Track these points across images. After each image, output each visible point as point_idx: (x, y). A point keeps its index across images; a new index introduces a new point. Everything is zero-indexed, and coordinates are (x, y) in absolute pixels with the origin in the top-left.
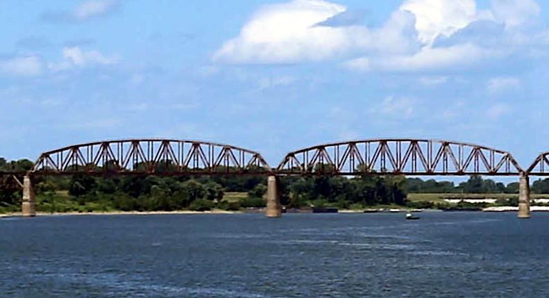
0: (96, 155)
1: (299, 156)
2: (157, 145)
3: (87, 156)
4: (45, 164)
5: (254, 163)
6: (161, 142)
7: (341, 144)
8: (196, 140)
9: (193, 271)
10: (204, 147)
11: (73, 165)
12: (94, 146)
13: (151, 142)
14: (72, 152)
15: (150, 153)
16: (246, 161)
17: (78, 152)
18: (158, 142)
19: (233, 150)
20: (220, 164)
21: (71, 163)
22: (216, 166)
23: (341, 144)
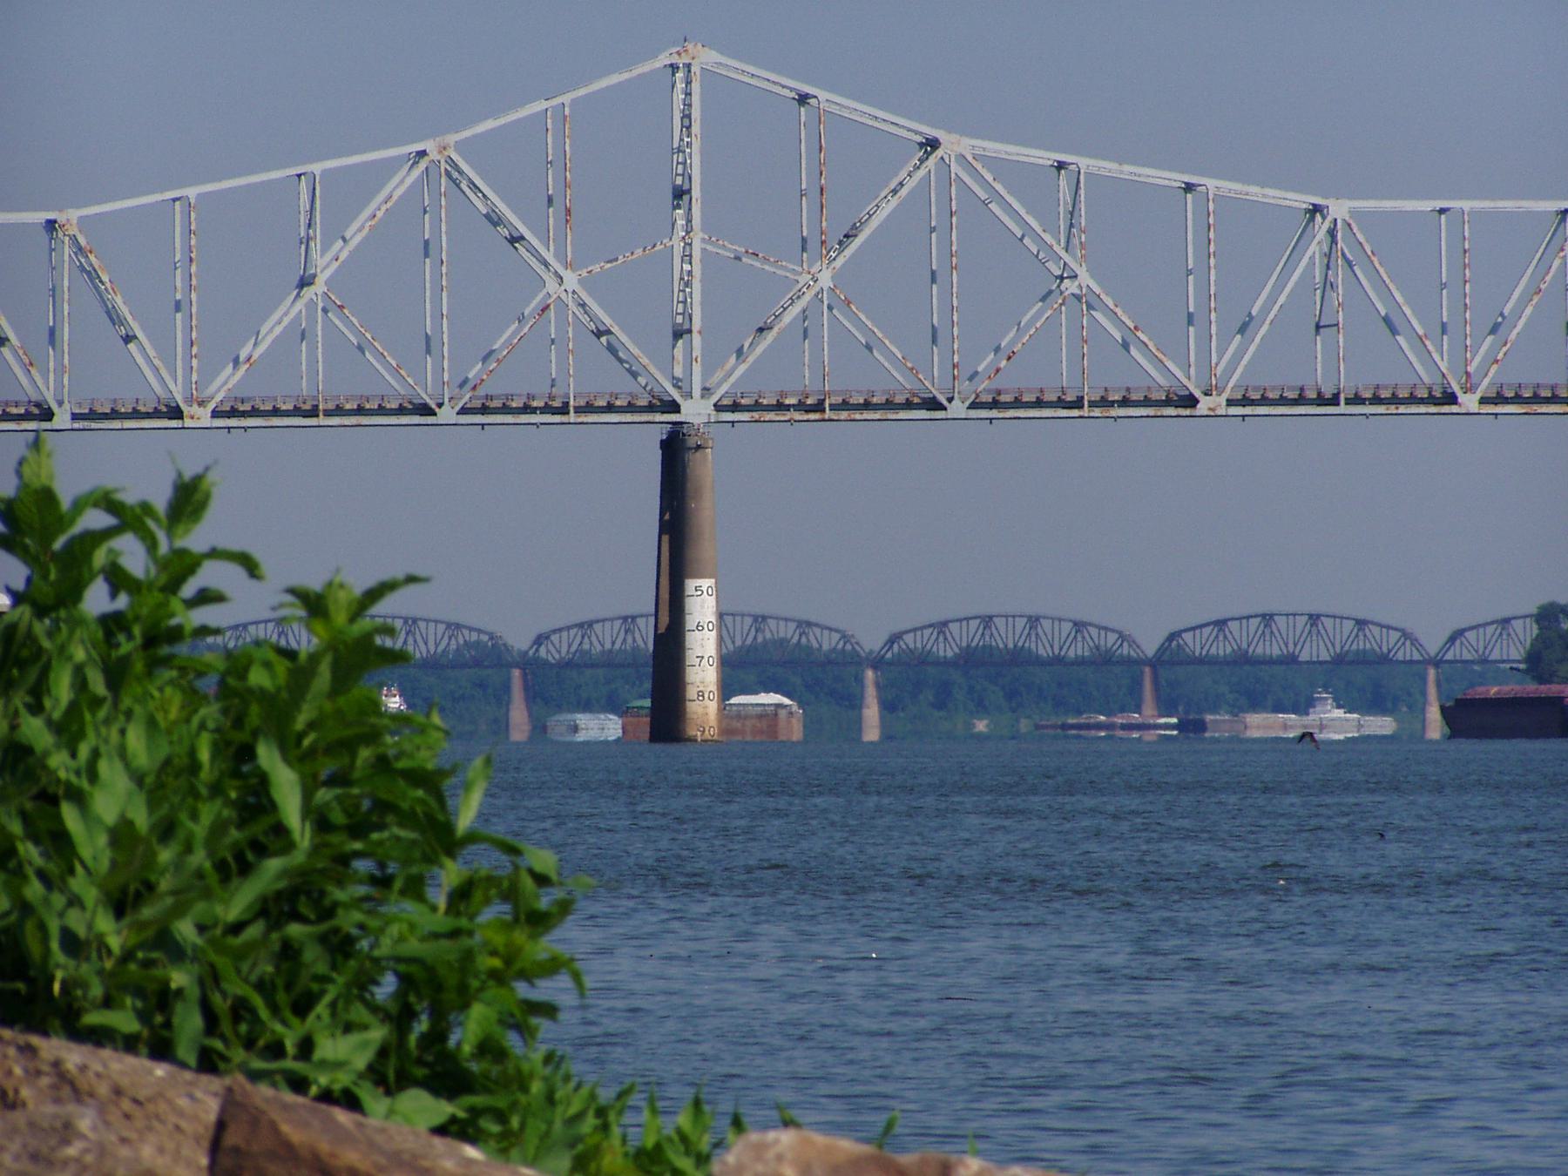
0: (974, 631)
1: (909, 638)
2: (1021, 623)
3: (1007, 636)
4: (1361, 643)
5: (1119, 651)
6: (1026, 619)
7: (1252, 617)
8: (1314, 610)
9: (405, 980)
10: (1000, 622)
11: (1358, 650)
12: (971, 622)
13: (1010, 619)
14: (935, 633)
15: (964, 636)
16: (828, 642)
17: (1511, 630)
18: (1021, 619)
19: (1090, 628)
20: (1210, 652)
21: (1354, 647)
22: (753, 648)
23: (1252, 617)
